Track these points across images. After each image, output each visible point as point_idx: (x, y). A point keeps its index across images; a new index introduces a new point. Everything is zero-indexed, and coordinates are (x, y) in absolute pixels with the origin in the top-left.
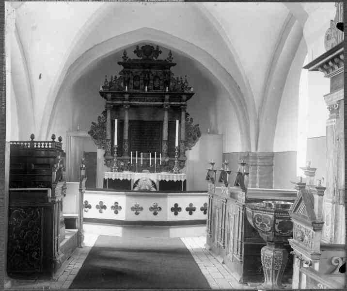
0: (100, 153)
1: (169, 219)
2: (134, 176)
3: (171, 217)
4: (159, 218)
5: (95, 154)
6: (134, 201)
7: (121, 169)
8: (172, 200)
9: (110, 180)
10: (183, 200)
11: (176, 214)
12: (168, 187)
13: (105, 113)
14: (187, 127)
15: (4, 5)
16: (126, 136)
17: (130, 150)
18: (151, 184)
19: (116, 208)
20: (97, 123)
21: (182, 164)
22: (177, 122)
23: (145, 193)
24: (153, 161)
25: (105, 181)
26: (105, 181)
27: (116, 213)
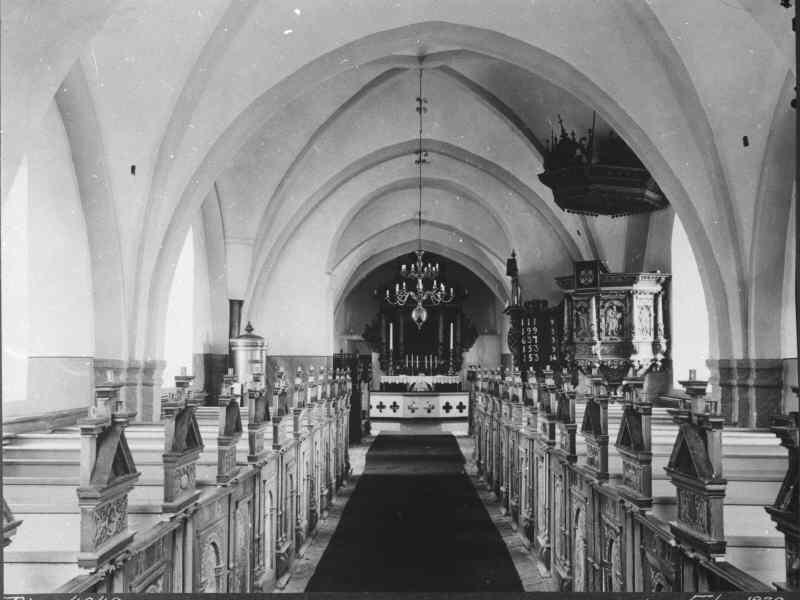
0: (375, 356)
2: (410, 380)
3: (443, 414)
4: (432, 415)
5: (369, 358)
6: (409, 400)
7: (397, 373)
8: (443, 399)
9: (387, 384)
13: (379, 315)
16: (402, 340)
18: (426, 387)
19: (395, 406)
21: (458, 367)
27: (461, 411)
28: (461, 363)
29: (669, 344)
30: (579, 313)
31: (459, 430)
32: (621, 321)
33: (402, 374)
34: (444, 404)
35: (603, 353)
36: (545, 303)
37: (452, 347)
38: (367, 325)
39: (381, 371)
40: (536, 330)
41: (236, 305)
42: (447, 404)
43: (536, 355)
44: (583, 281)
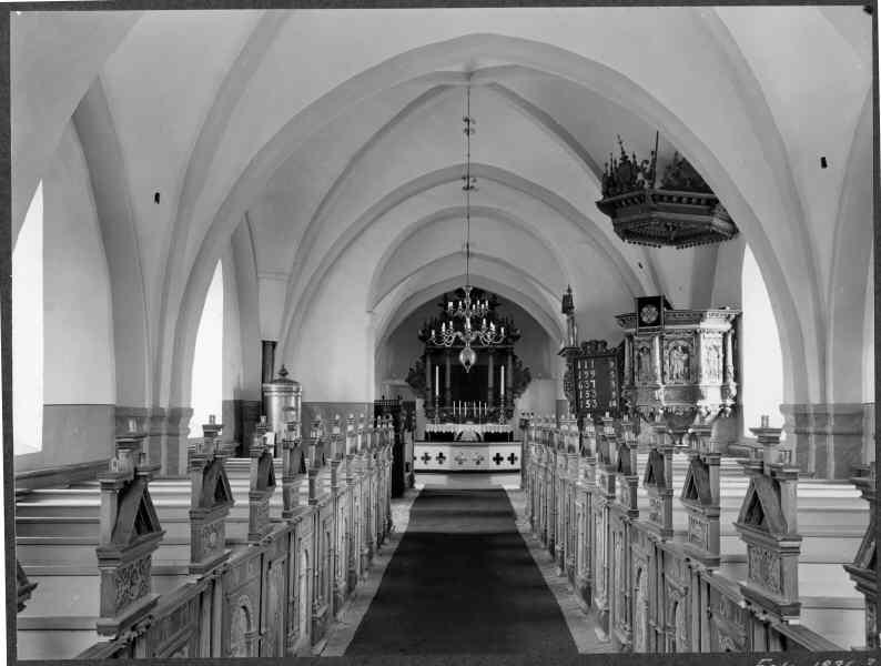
0: (419, 403)
1: (491, 468)
3: (493, 466)
5: (413, 405)
6: (457, 451)
7: (443, 421)
8: (494, 449)
9: (432, 433)
10: (506, 450)
11: (498, 463)
12: (491, 438)
14: (515, 371)
15: (582, 655)
16: (448, 384)
17: (452, 400)
18: (475, 435)
19: (441, 457)
20: (415, 369)
21: (509, 415)
22: (503, 368)
23: (470, 444)
24: (478, 411)
25: (426, 434)
26: (426, 434)
29: (739, 388)
31: (510, 483)
32: (687, 363)
34: (495, 455)
35: (667, 398)
37: (502, 393)
38: (411, 369)
40: (593, 373)
41: (269, 347)
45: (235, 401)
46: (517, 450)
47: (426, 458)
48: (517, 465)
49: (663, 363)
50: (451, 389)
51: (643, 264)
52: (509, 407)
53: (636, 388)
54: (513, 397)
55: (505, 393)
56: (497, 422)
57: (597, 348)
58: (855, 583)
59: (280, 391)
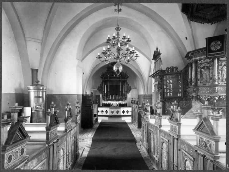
0: (101, 95)
2: (111, 102)
3: (122, 114)
4: (119, 114)
7: (107, 100)
8: (122, 109)
9: (104, 104)
10: (125, 109)
13: (102, 83)
14: (127, 87)
16: (109, 90)
18: (116, 105)
19: (106, 112)
21: (126, 99)
23: (115, 107)
24: (117, 98)
28: (126, 98)
30: (203, 70)
31: (128, 120)
33: (109, 101)
34: (122, 111)
36: (176, 68)
37: (124, 93)
39: (103, 100)
40: (171, 81)
41: (34, 72)
42: (124, 111)
43: (171, 94)
44: (212, 49)
45: (16, 94)
46: (130, 109)
47: (102, 112)
48: (130, 114)
49: (218, 73)
50: (110, 92)
51: (187, 38)
52: (126, 97)
53: (198, 87)
54: (127, 94)
55: (125, 93)
56: (123, 101)
57: (173, 70)
58: (194, 132)
59: (34, 89)
